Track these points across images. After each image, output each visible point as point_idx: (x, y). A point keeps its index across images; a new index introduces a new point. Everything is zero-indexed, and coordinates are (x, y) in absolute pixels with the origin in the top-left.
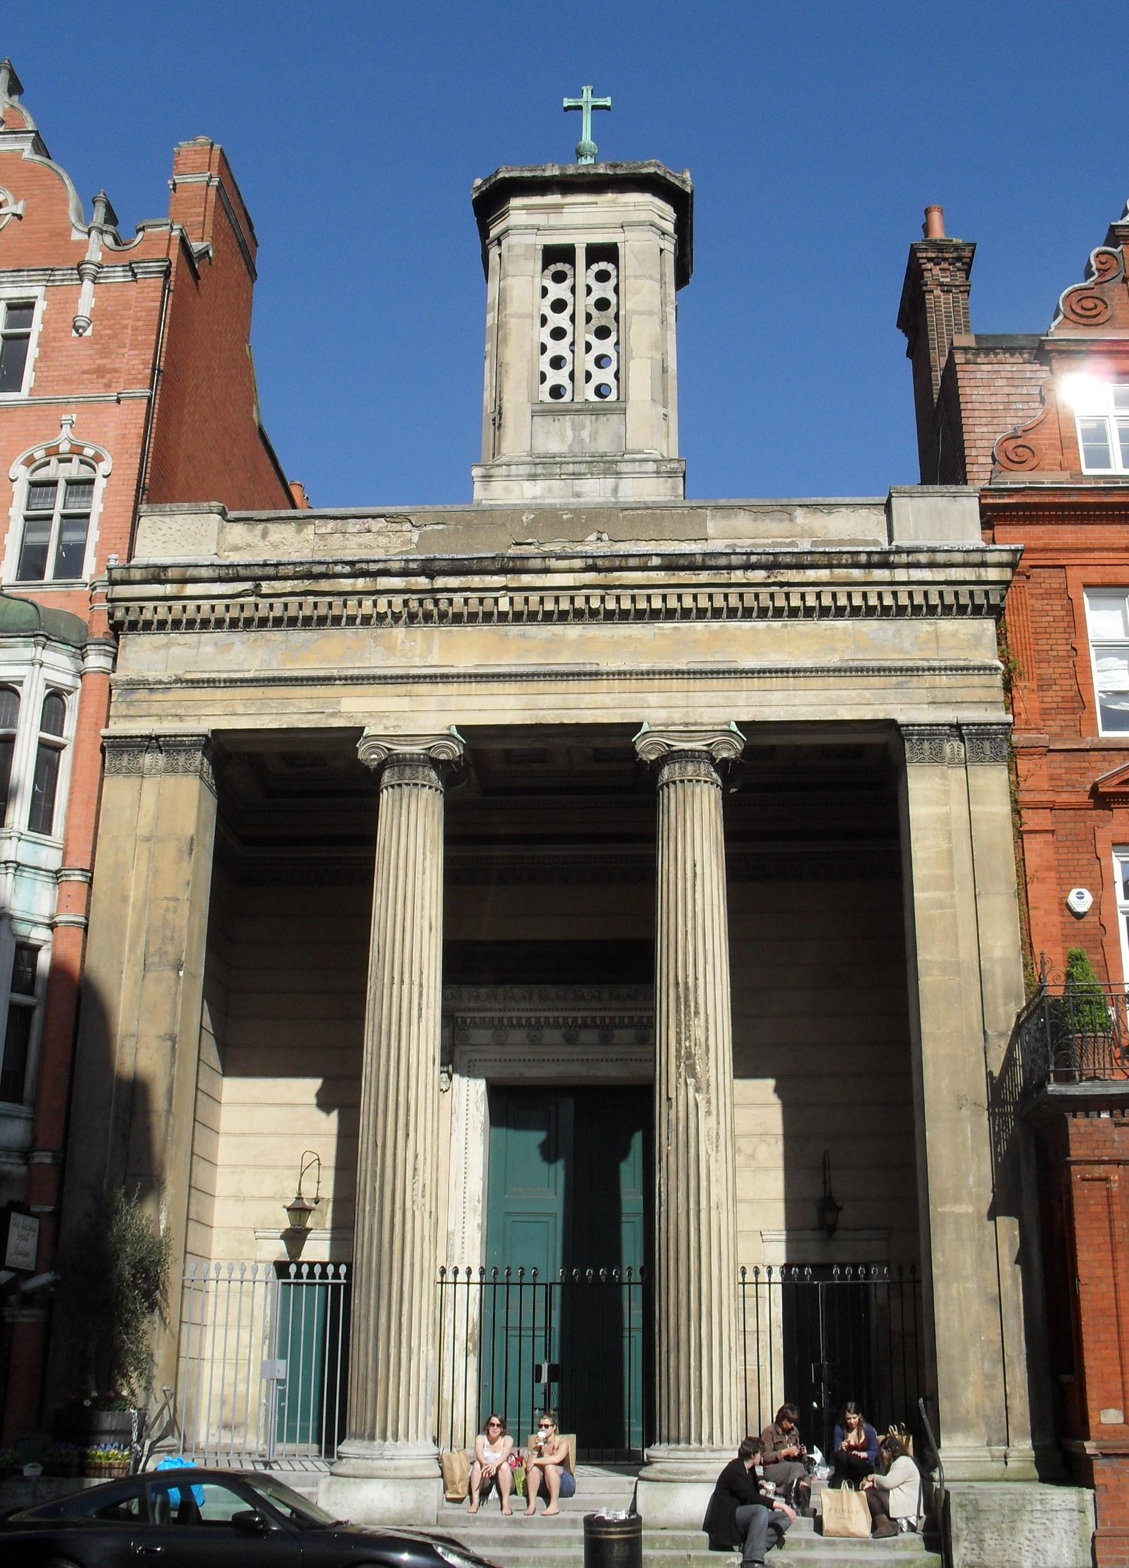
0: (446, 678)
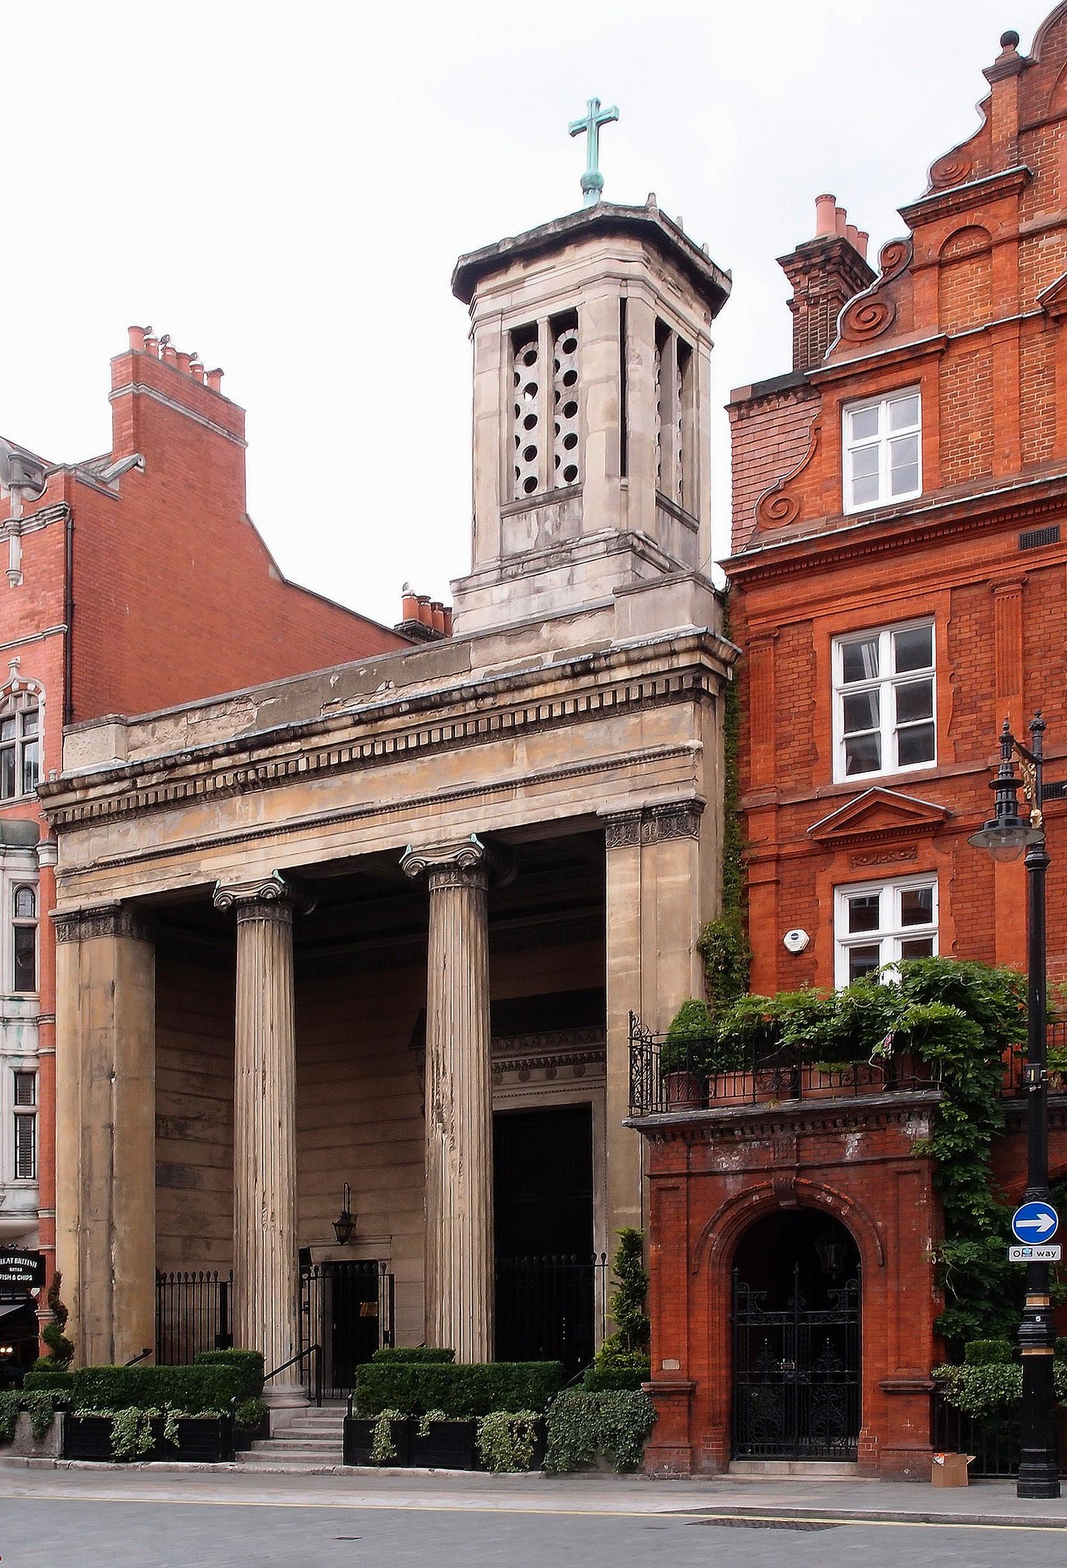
0: (268, 833)
